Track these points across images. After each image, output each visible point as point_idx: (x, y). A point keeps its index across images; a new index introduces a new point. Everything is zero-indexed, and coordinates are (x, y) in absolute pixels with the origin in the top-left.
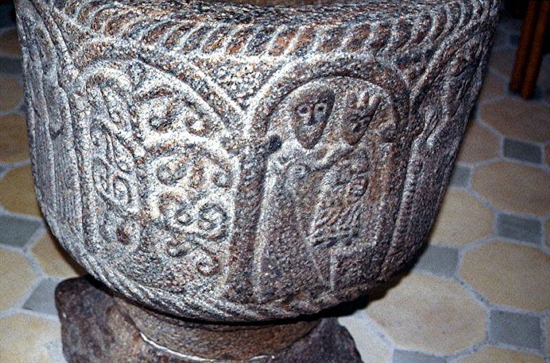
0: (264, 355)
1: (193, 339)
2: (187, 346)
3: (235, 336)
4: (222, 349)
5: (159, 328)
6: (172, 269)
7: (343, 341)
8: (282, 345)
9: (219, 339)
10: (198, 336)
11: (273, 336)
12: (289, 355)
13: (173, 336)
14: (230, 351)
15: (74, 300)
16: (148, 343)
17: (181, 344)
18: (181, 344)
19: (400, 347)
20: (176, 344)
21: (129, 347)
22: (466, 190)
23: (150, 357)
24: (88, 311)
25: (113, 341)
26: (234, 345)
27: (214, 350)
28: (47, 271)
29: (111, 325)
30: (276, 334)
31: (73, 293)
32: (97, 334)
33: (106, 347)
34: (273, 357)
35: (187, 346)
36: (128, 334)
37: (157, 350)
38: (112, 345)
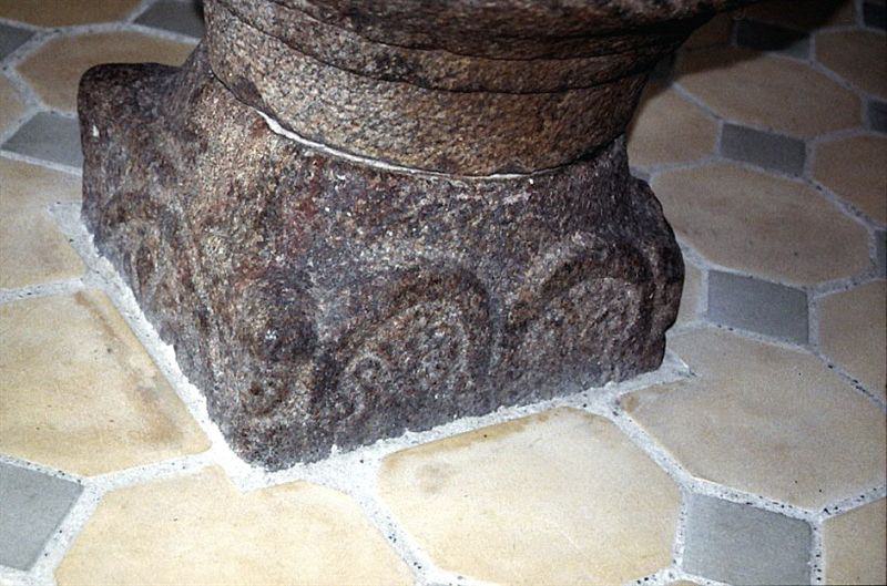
0: (516, 173)
1: (383, 116)
2: (368, 133)
3: (472, 112)
4: (439, 142)
5: (315, 92)
6: (134, 475)
7: (642, 201)
8: (552, 155)
9: (439, 116)
10: (394, 109)
11: (540, 129)
12: (560, 184)
13: (341, 110)
14: (454, 149)
15: (119, 95)
16: (284, 137)
17: (356, 130)
18: (356, 130)
19: (717, 267)
20: (345, 129)
21: (240, 152)
22: (806, 62)
23: (289, 159)
24: (147, 114)
25: (205, 147)
26: (465, 136)
27: (423, 144)
28: (47, 101)
29: (202, 121)
30: (547, 124)
31: (117, 84)
32: (171, 146)
33: (187, 165)
34: (531, 181)
35: (368, 133)
36: (239, 128)
37: (301, 146)
38: (202, 157)
